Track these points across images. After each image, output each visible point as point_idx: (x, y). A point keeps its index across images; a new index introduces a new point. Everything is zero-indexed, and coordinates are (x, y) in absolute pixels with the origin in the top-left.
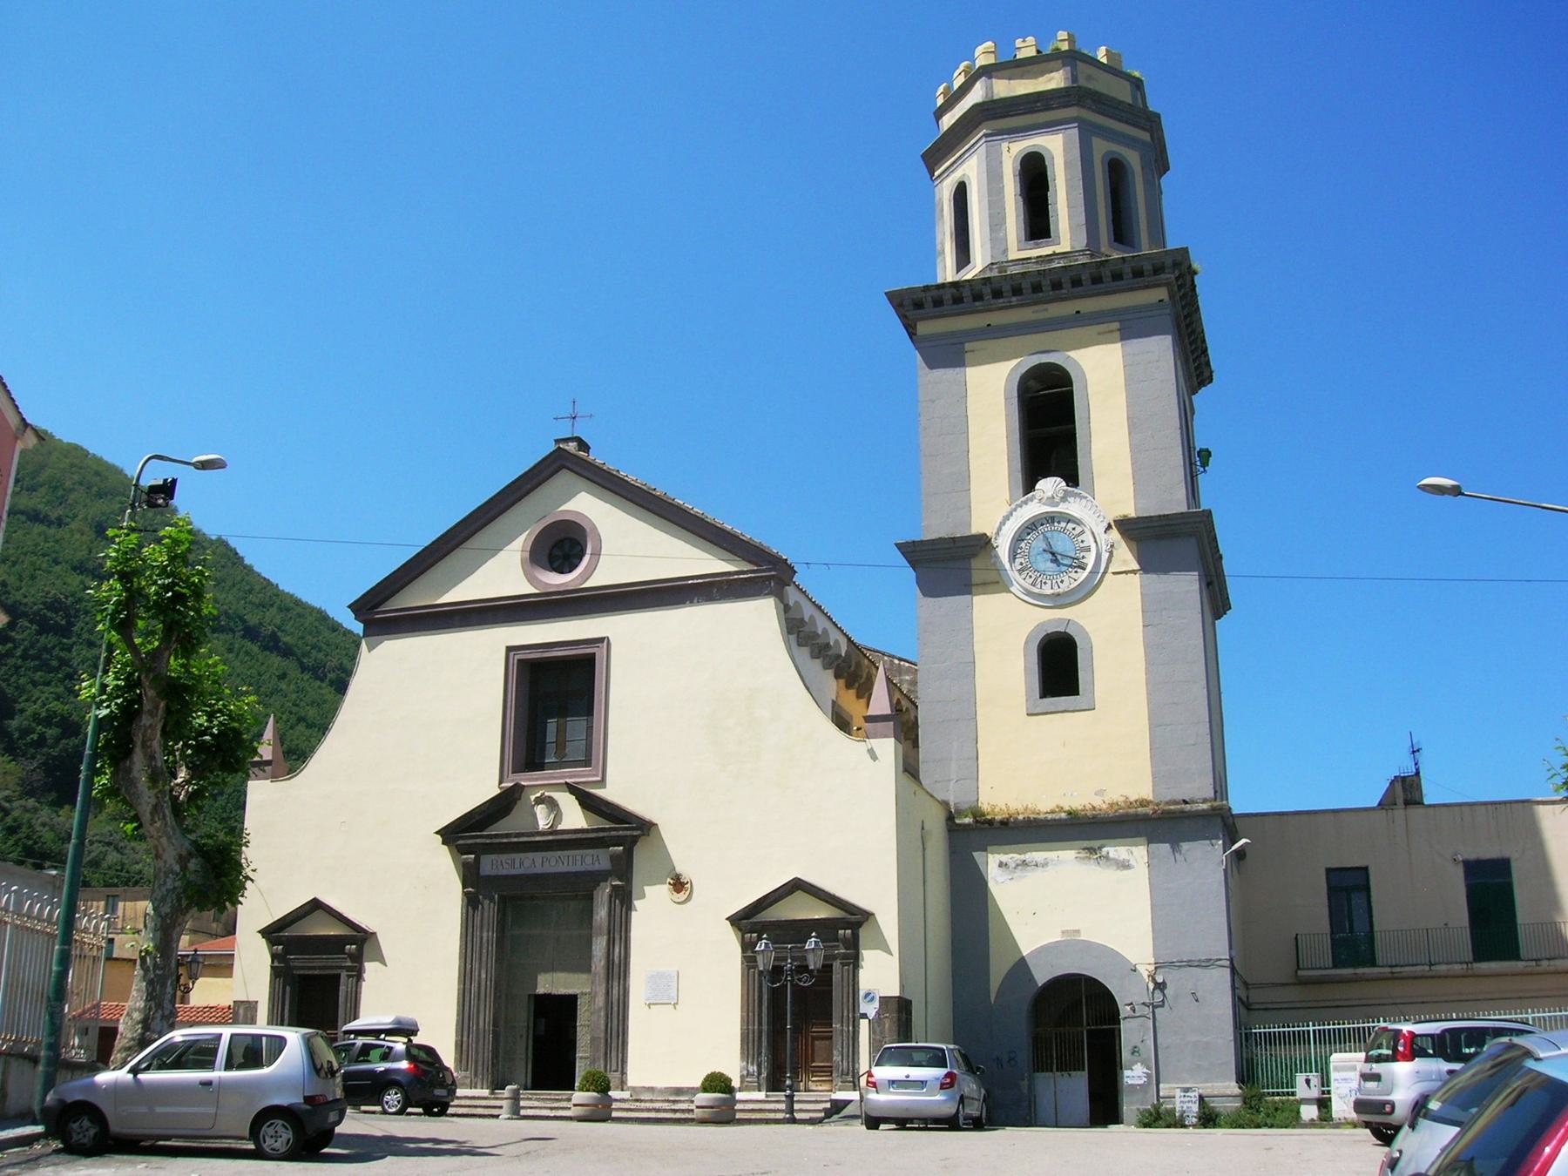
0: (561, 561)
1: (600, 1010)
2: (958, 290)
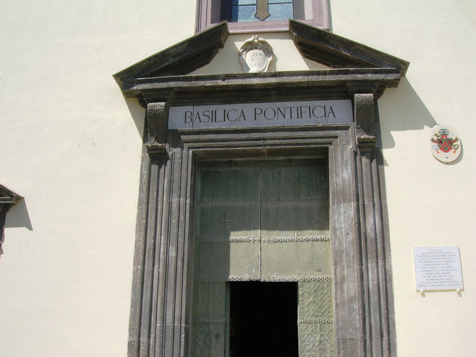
1: (351, 300)
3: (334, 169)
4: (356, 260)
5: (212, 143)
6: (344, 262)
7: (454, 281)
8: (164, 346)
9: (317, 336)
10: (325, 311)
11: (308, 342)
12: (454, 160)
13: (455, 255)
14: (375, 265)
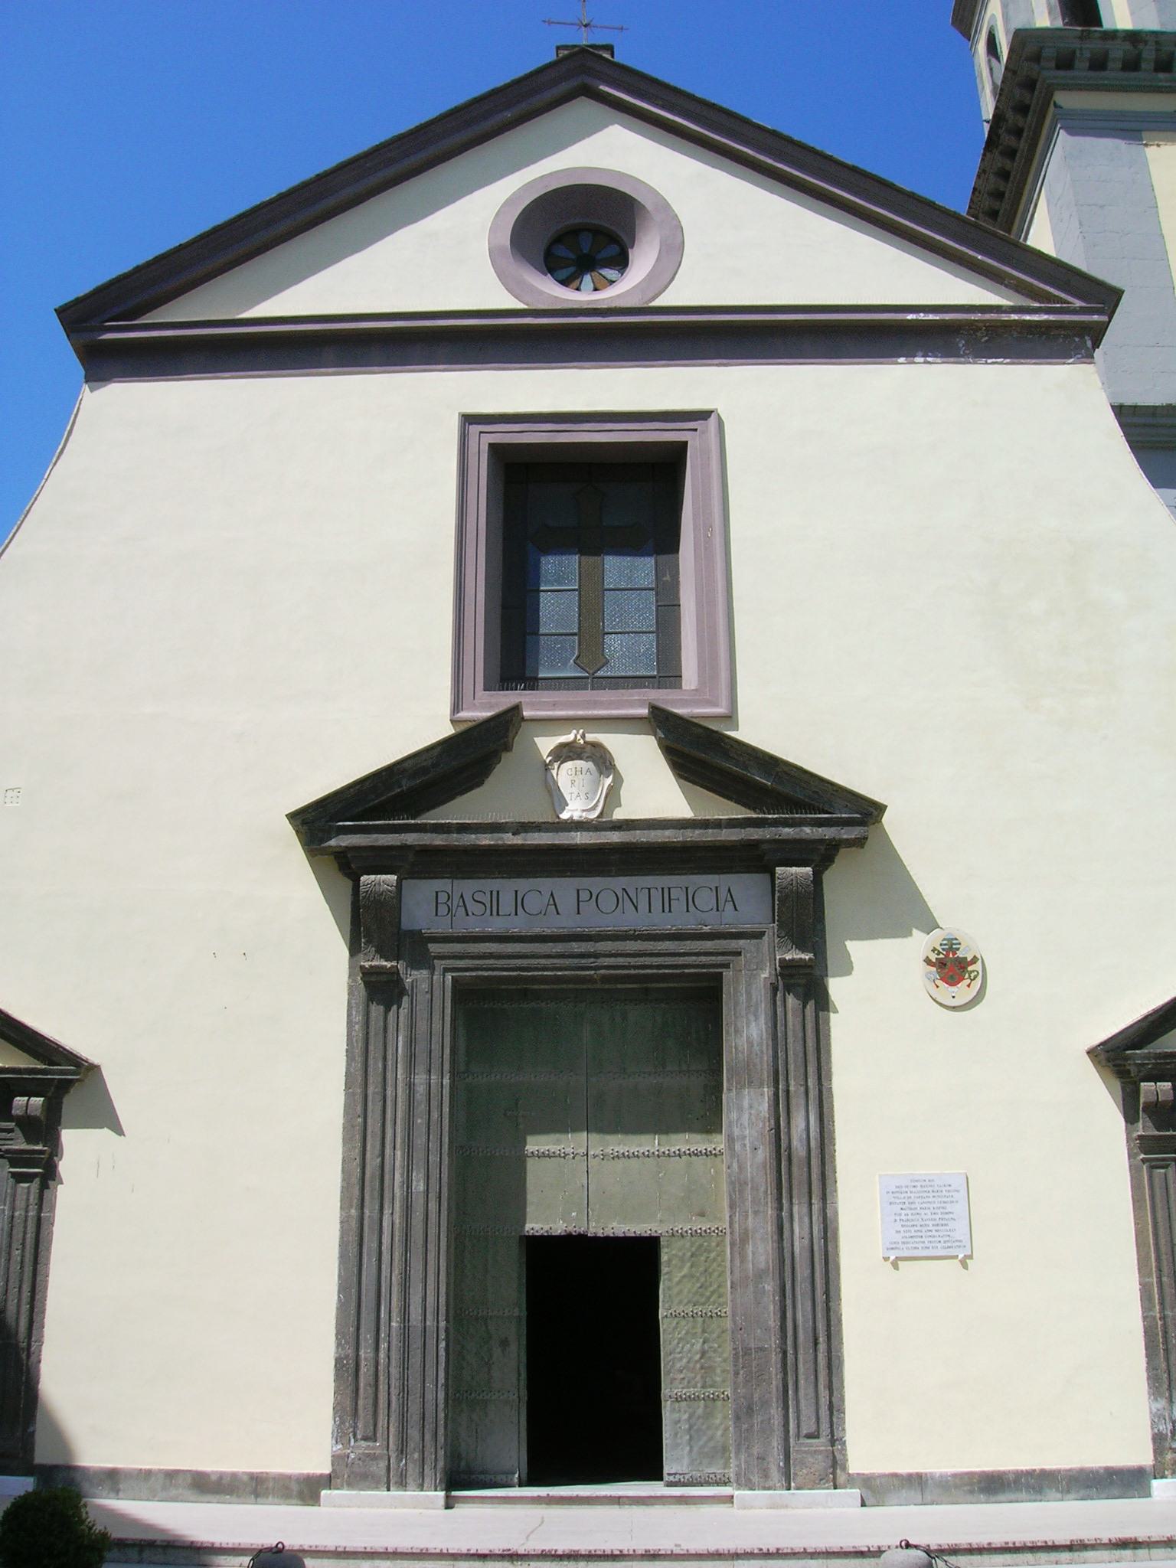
0: (572, 256)
1: (760, 1276)
2: (1135, 47)
3: (733, 1018)
4: (769, 1200)
5: (491, 961)
6: (749, 1204)
7: (954, 1240)
8: (406, 1366)
9: (698, 1342)
10: (713, 1293)
11: (680, 1353)
12: (962, 1003)
13: (958, 1191)
14: (805, 1210)
